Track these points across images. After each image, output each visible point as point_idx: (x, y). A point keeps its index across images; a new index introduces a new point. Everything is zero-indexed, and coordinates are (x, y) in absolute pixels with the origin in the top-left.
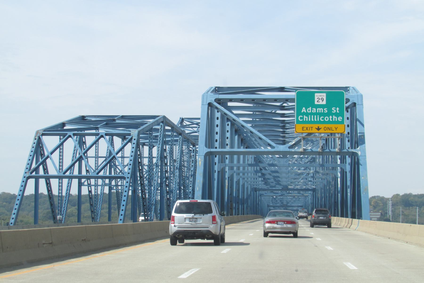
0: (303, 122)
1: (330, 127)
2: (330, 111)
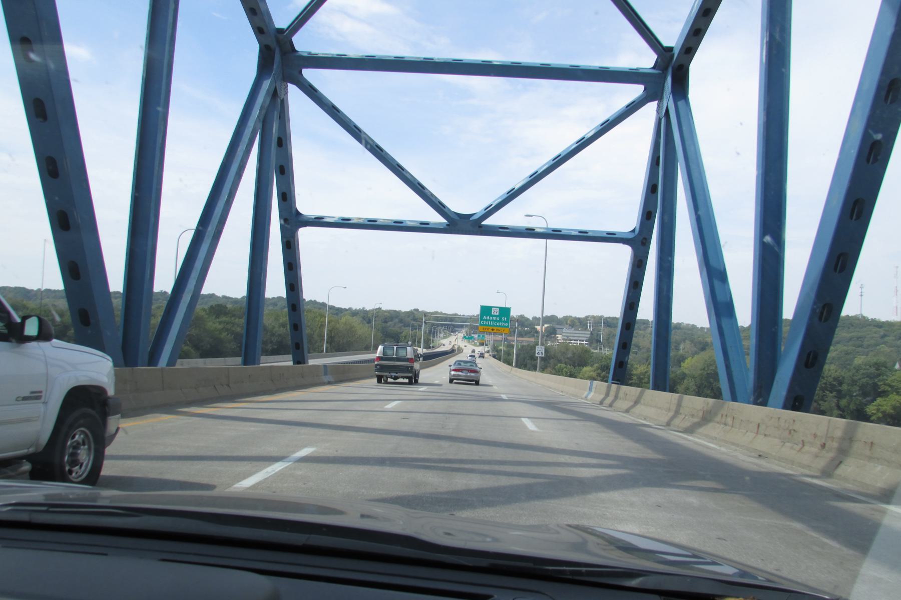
0: (484, 325)
2: (501, 319)
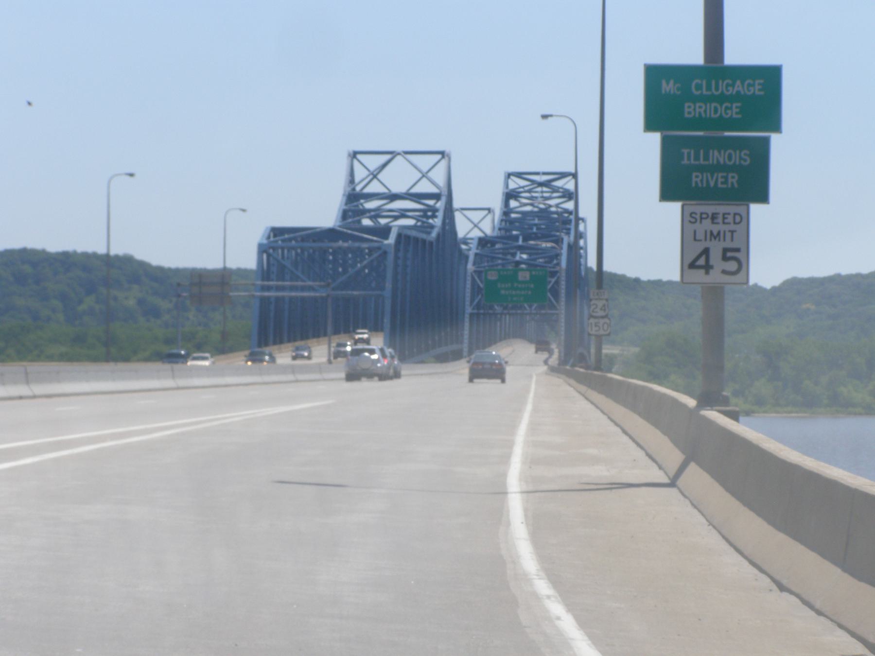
1: (711, 240)
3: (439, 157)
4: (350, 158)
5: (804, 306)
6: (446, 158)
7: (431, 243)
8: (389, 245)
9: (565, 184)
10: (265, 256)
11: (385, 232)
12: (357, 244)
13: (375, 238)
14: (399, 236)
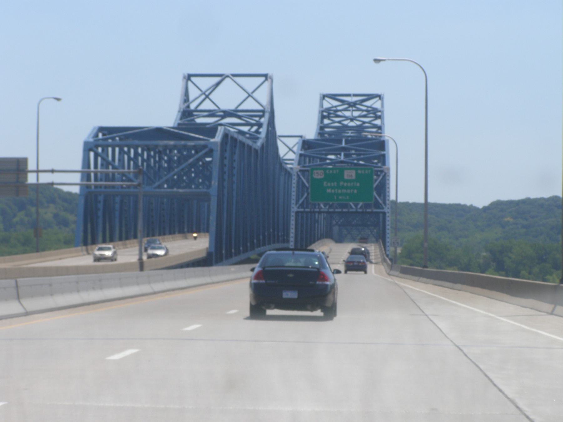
3: (263, 79)
4: (185, 80)
5: (506, 219)
6: (269, 80)
7: (256, 151)
8: (215, 143)
9: (373, 104)
10: (92, 154)
11: (211, 131)
12: (183, 143)
13: (201, 137)
14: (226, 136)
